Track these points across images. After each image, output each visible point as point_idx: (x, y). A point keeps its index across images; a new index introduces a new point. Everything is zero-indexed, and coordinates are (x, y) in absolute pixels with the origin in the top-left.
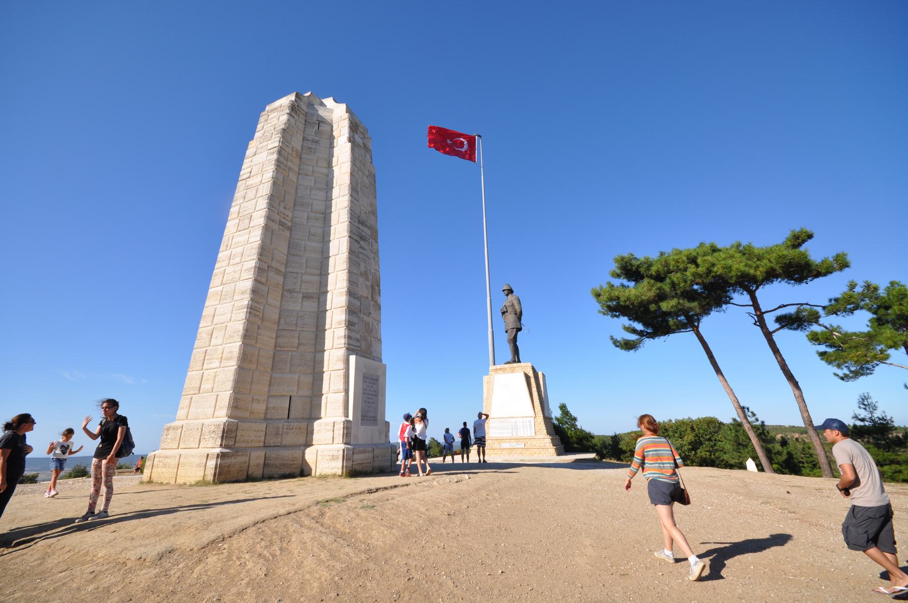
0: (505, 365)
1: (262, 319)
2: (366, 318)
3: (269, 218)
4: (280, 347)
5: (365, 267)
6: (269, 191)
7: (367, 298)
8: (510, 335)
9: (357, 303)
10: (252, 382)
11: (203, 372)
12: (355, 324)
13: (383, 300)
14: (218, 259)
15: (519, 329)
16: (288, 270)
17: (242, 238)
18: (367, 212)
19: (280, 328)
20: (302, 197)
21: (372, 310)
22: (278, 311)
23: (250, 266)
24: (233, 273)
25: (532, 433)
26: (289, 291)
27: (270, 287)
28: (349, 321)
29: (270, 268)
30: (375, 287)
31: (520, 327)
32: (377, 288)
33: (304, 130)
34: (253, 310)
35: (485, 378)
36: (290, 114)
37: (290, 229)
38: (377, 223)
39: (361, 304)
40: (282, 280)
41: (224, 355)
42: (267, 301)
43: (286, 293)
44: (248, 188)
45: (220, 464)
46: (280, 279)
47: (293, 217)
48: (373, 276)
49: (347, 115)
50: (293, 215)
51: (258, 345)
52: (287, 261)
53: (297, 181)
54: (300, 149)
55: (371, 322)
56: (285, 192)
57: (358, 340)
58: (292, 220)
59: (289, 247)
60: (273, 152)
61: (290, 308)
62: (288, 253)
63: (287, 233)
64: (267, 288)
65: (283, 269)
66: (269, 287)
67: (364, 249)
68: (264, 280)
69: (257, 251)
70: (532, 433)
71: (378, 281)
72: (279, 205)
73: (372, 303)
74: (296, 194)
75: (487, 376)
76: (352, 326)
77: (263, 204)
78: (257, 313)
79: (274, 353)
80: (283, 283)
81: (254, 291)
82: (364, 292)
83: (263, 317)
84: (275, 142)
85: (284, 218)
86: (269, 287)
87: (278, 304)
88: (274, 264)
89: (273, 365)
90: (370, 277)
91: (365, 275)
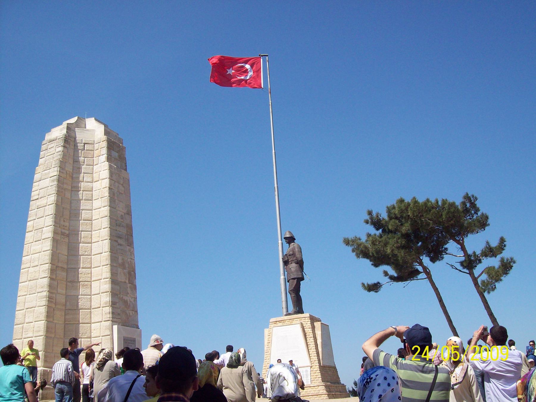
0: (286, 317)
1: (56, 304)
2: (125, 298)
3: (55, 232)
4: (68, 322)
5: (123, 259)
6: (53, 211)
7: (125, 282)
8: (292, 285)
9: (117, 287)
10: (53, 345)
11: (23, 340)
12: (117, 303)
13: (139, 282)
14: (23, 262)
15: (302, 279)
16: (69, 267)
17: (37, 247)
18: (123, 214)
19: (67, 308)
20: (75, 209)
21: (129, 290)
22: (65, 296)
23: (45, 269)
24: (34, 273)
25: (308, 382)
26: (70, 282)
27: (58, 282)
28: (112, 302)
29: (57, 268)
30: (132, 275)
31: (300, 276)
32: (132, 273)
33: (74, 153)
34: (50, 299)
35: (266, 331)
36: (64, 147)
37: (68, 236)
38: (131, 221)
39: (120, 288)
40: (66, 275)
41: (35, 329)
42: (57, 290)
43: (69, 284)
44: (38, 207)
45: (42, 393)
46: (64, 274)
47: (69, 226)
48: (129, 264)
49: (105, 138)
50: (69, 224)
51: (55, 321)
52: (68, 260)
53: (71, 197)
54: (71, 171)
55: (129, 301)
56: (63, 209)
57: (119, 314)
58: (69, 229)
59: (68, 250)
60: (54, 180)
61: (72, 294)
62: (68, 254)
63: (66, 240)
64: (57, 283)
65: (65, 266)
66: (57, 281)
67: (121, 245)
68: (54, 277)
69: (48, 257)
70: (308, 382)
71: (134, 267)
72: (60, 220)
73: (129, 285)
74: (71, 207)
75: (267, 329)
76: (114, 305)
77: (49, 221)
78: (52, 300)
79: (65, 326)
80: (67, 276)
81: (50, 286)
82: (122, 278)
83: (56, 302)
84: (55, 172)
85: (64, 229)
86: (57, 281)
87: (64, 292)
88: (60, 265)
89: (64, 334)
90: (127, 266)
91: (123, 265)
